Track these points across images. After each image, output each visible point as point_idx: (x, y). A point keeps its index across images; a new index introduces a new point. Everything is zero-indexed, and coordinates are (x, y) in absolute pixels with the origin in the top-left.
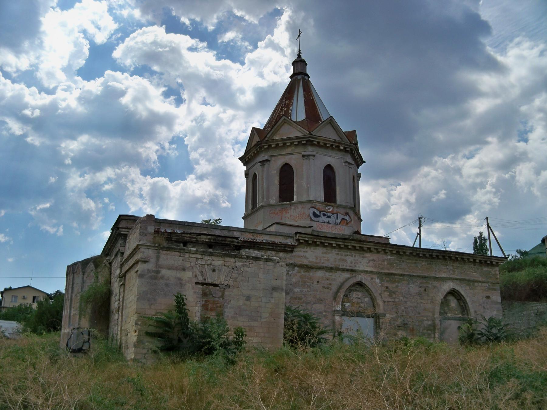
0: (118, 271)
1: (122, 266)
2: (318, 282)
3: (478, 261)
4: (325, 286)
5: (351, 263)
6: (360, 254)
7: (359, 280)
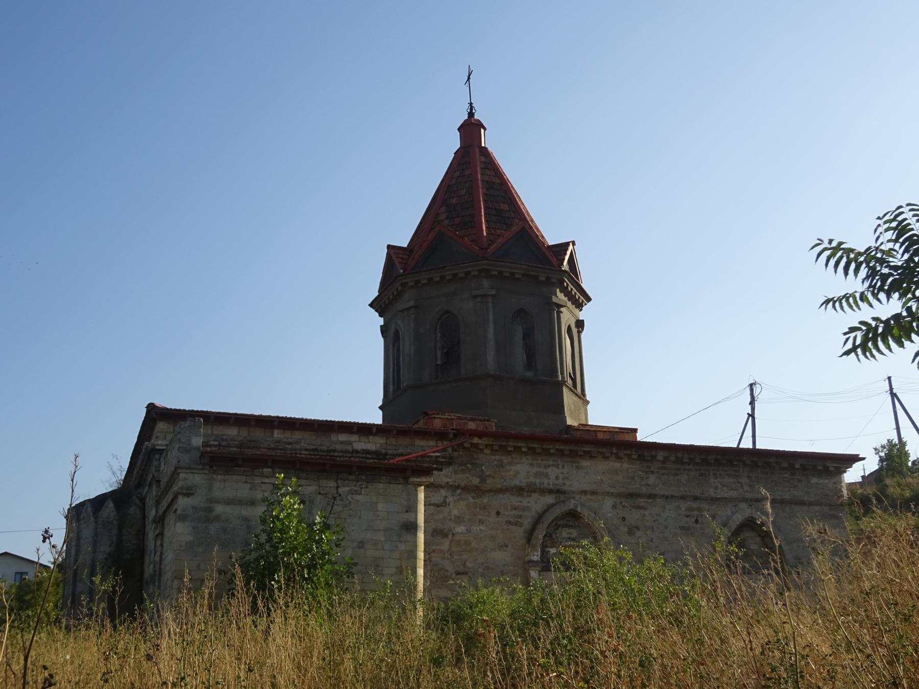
0: (153, 512)
1: (158, 503)
2: (498, 513)
3: (797, 466)
4: (512, 520)
5: (557, 478)
6: (573, 462)
7: (572, 507)
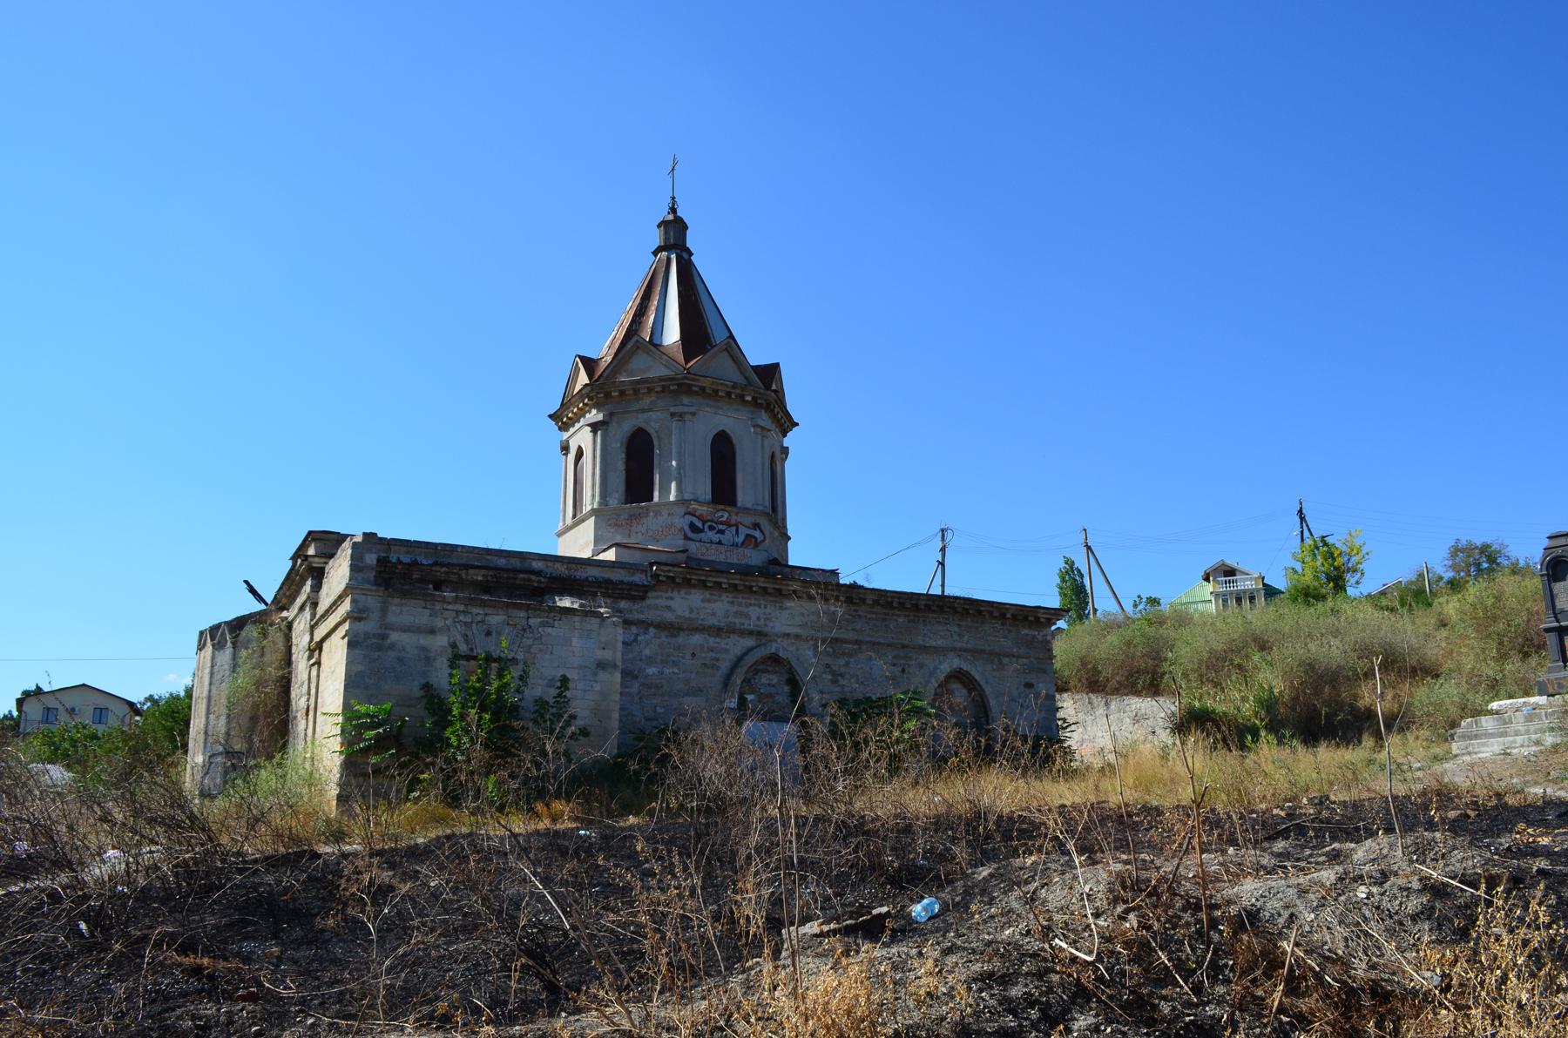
2: (693, 655)
